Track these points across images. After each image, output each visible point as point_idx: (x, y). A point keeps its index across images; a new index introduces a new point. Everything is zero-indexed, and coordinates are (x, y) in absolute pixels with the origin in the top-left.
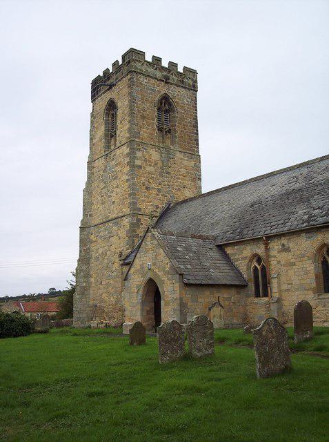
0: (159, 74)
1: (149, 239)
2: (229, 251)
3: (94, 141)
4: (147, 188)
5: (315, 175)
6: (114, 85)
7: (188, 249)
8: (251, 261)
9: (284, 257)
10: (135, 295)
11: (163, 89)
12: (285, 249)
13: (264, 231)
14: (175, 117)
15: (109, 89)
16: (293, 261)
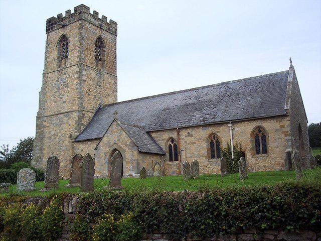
0: (97, 23)
1: (114, 126)
2: (153, 135)
3: (48, 60)
4: (88, 95)
5: (201, 96)
6: (66, 26)
7: (134, 132)
8: (168, 141)
9: (189, 139)
10: (103, 158)
11: (99, 33)
12: (189, 135)
13: (176, 125)
14: (104, 51)
15: (62, 28)
16: (194, 141)
